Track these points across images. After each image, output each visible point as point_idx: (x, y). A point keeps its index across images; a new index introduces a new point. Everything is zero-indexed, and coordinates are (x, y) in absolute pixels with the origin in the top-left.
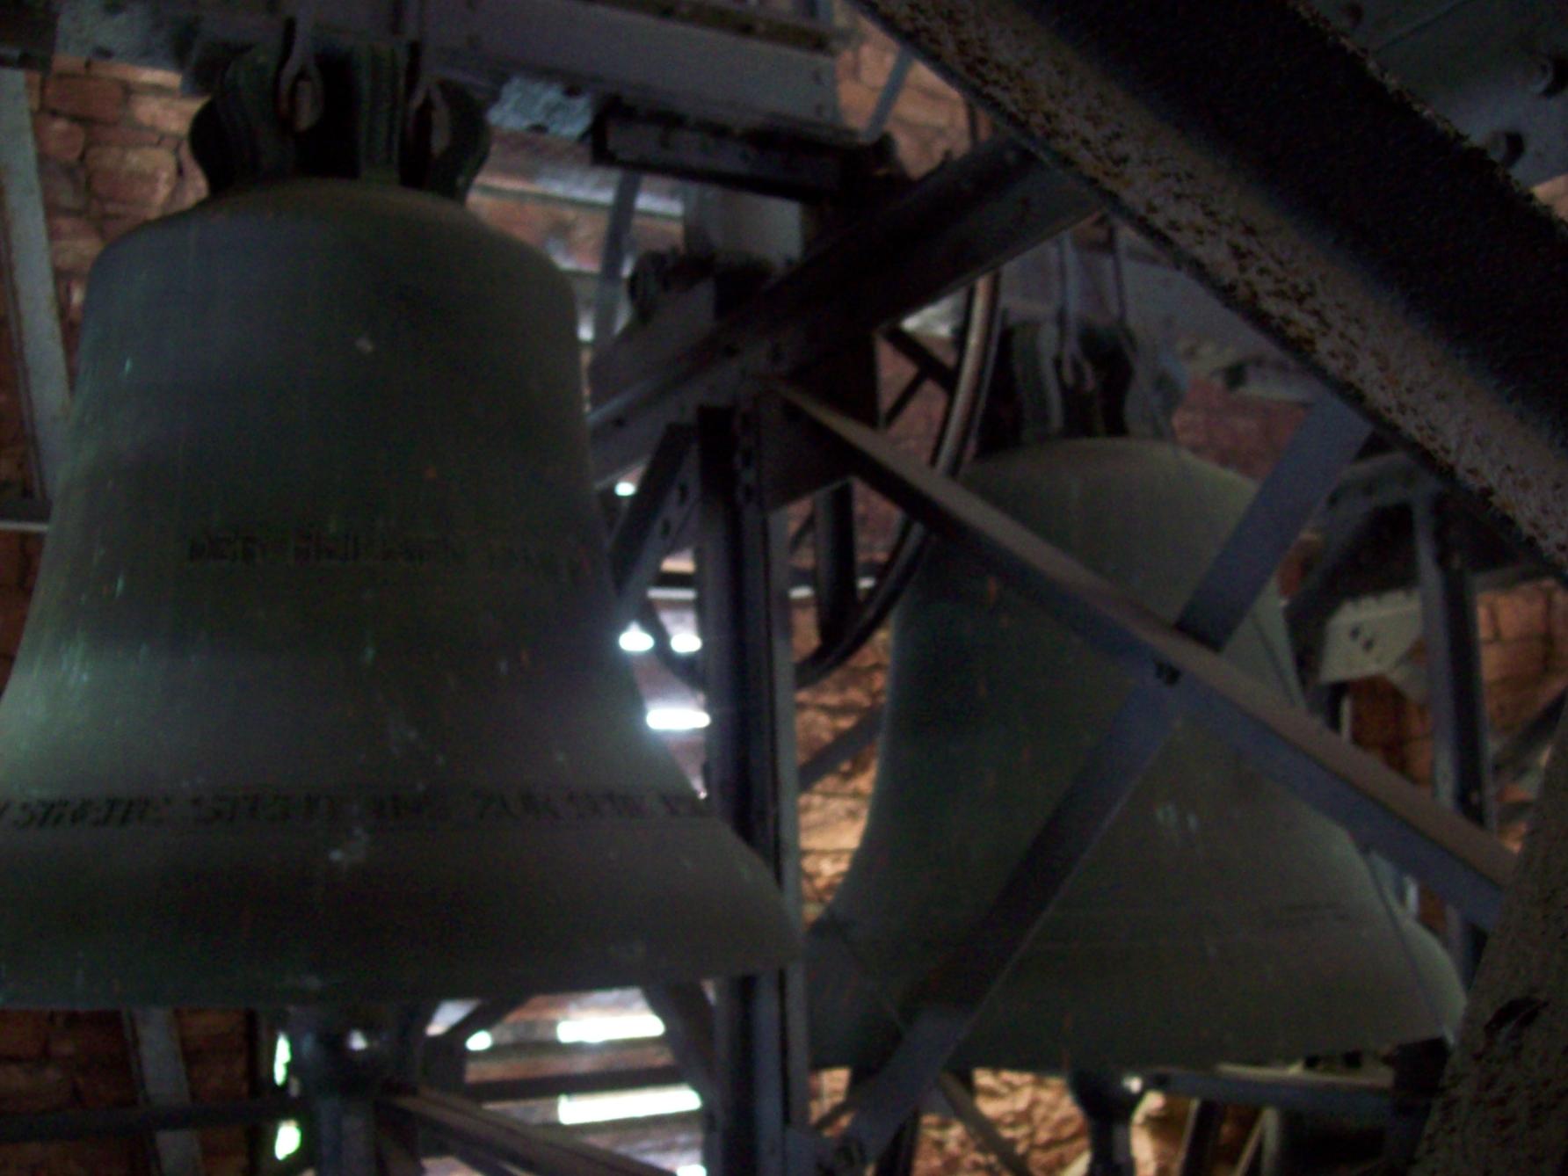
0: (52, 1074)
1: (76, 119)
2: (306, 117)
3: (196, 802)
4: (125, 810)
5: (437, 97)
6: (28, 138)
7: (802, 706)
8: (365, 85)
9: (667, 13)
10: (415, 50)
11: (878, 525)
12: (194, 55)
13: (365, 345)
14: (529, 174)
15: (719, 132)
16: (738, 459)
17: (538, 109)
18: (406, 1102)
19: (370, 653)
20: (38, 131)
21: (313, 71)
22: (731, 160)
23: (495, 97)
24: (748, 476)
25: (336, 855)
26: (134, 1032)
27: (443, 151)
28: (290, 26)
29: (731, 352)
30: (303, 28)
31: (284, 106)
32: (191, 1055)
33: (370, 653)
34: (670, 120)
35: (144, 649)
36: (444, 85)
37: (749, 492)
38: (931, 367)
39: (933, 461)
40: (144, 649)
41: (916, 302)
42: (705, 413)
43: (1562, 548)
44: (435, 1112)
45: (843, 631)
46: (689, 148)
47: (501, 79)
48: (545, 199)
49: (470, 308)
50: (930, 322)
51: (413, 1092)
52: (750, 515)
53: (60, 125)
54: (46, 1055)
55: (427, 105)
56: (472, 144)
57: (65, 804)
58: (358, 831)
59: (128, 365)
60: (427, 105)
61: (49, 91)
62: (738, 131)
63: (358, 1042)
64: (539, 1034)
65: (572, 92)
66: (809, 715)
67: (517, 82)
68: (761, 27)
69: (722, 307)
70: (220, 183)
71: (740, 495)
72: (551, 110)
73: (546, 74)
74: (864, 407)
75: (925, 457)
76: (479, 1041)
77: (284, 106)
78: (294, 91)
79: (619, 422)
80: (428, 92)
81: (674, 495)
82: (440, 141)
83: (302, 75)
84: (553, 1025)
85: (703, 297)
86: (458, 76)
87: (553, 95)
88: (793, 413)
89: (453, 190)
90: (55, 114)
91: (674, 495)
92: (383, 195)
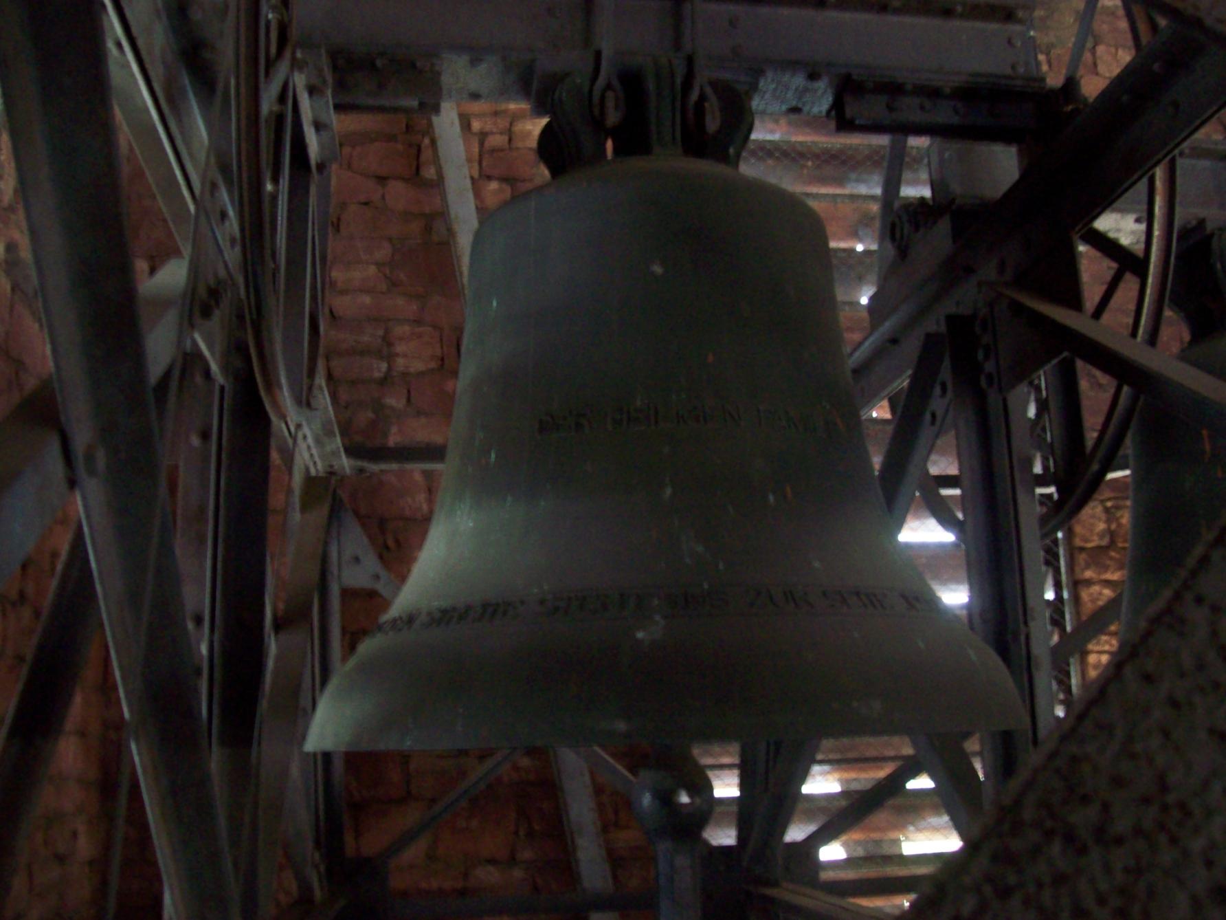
0: (518, 873)
1: (504, 179)
2: (613, 117)
3: (542, 602)
4: (492, 610)
5: (708, 90)
6: (471, 195)
7: (1089, 583)
8: (651, 86)
9: (884, 9)
10: (690, 60)
11: (1096, 392)
12: (535, 85)
13: (657, 269)
14: (840, 182)
15: (934, 93)
16: (980, 355)
17: (790, 94)
18: (769, 892)
19: (668, 491)
20: (477, 194)
21: (616, 83)
22: (944, 114)
23: (754, 88)
24: (989, 366)
25: (640, 635)
26: (573, 842)
27: (716, 130)
28: (598, 55)
29: (969, 271)
30: (607, 54)
31: (596, 111)
32: (616, 860)
33: (668, 491)
34: (893, 89)
35: (509, 498)
36: (714, 84)
37: (990, 377)
38: (1128, 262)
39: (1134, 334)
40: (509, 498)
41: (1104, 203)
42: (951, 320)
43: (1220, 21)
44: (789, 897)
45: (1077, 481)
46: (910, 109)
47: (758, 72)
48: (853, 197)
49: (763, 260)
50: (1120, 225)
51: (775, 884)
52: (993, 399)
53: (494, 185)
54: (512, 860)
55: (702, 98)
56: (738, 118)
57: (454, 609)
58: (657, 618)
59: (495, 304)
60: (702, 98)
61: (484, 164)
62: (948, 91)
63: (685, 799)
64: (887, 850)
65: (813, 76)
66: (1096, 589)
67: (770, 74)
68: (959, 9)
69: (957, 233)
70: (556, 172)
71: (983, 383)
72: (801, 93)
73: (791, 65)
74: (1072, 297)
75: (1126, 332)
76: (832, 852)
77: (596, 111)
78: (603, 98)
79: (894, 341)
80: (701, 89)
81: (937, 390)
82: (712, 124)
83: (609, 86)
84: (897, 842)
85: (943, 227)
86: (727, 76)
87: (799, 80)
88: (1018, 309)
89: (736, 165)
90: (489, 178)
91: (937, 390)
92: (668, 161)
